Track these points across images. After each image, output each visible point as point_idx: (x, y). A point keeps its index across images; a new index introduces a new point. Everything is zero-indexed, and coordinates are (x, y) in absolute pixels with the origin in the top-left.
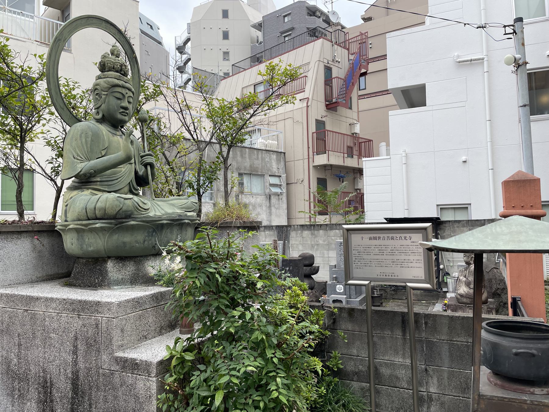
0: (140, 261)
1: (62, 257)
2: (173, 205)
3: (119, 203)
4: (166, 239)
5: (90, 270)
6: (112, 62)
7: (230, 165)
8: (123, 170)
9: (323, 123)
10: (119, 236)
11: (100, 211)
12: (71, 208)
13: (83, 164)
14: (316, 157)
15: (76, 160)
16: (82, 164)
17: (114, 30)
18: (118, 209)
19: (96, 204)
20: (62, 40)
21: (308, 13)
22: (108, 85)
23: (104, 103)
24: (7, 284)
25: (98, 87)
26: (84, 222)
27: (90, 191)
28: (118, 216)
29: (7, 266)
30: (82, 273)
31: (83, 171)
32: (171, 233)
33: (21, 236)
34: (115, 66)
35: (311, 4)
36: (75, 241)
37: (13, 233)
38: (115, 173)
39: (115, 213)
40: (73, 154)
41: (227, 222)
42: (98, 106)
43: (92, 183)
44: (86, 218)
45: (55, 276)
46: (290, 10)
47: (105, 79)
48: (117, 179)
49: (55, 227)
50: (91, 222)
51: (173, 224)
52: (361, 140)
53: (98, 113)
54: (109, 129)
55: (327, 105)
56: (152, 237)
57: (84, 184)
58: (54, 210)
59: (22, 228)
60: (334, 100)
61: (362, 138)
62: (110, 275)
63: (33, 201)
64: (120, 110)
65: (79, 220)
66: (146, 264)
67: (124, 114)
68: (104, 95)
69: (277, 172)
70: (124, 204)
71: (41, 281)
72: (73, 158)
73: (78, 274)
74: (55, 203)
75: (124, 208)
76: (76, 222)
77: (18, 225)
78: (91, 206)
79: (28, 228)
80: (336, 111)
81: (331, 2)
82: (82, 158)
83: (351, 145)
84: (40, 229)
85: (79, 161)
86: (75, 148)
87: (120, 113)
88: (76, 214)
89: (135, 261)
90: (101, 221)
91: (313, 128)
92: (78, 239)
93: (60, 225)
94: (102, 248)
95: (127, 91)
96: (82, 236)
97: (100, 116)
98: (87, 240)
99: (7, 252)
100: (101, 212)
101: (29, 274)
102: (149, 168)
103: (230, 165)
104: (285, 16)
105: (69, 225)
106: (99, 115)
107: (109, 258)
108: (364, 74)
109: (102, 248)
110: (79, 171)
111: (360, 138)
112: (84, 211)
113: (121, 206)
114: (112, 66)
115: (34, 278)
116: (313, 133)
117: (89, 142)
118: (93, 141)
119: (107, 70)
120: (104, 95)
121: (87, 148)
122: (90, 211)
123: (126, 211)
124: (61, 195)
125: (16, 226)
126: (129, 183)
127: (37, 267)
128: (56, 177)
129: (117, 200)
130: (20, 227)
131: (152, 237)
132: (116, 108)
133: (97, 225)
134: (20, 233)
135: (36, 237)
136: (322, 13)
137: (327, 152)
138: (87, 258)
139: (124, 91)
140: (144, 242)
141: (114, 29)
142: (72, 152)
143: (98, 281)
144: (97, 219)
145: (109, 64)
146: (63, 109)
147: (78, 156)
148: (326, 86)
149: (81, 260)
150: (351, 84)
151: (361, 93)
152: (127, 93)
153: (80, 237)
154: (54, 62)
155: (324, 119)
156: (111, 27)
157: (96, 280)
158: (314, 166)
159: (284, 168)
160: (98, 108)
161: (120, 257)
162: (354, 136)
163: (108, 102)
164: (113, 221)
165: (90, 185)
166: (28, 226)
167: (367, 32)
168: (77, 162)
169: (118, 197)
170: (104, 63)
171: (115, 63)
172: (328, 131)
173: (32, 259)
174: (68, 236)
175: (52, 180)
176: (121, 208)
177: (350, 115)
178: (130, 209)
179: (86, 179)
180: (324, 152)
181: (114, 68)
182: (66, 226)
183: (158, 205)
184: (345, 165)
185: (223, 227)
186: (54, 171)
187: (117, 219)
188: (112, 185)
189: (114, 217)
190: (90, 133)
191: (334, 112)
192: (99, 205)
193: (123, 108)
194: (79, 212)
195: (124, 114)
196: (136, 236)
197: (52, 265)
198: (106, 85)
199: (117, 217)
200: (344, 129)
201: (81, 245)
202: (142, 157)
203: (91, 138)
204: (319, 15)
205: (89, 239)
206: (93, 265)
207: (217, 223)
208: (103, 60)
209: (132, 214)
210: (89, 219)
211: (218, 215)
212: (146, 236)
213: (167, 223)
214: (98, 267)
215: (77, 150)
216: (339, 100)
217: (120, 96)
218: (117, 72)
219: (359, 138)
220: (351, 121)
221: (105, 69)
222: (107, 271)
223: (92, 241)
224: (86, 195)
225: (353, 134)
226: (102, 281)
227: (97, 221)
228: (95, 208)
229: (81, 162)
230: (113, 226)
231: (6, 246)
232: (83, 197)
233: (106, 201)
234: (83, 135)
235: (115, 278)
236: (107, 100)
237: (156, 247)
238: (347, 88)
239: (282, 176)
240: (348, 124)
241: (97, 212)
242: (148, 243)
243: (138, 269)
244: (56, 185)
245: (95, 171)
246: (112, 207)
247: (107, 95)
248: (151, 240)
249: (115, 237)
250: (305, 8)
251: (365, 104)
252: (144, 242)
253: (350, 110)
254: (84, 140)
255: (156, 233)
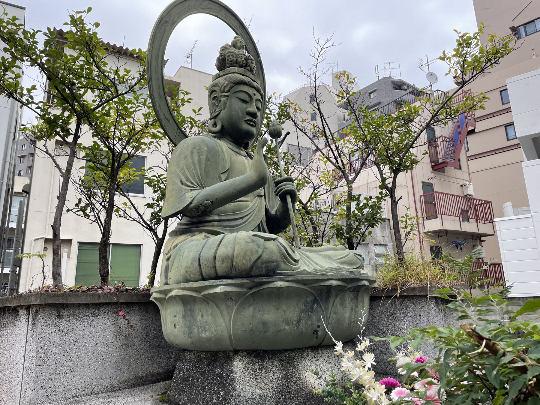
0: (291, 359)
1: (159, 346)
2: (329, 257)
3: (255, 247)
4: (335, 316)
5: (203, 374)
6: (235, 53)
7: (401, 198)
8: (251, 204)
9: (431, 185)
10: (254, 309)
11: (223, 263)
12: (175, 261)
13: (195, 193)
14: (426, 222)
15: (184, 187)
16: (193, 192)
17: (236, 23)
18: (254, 258)
19: (217, 250)
20: (170, 23)
21: (394, 87)
22: (230, 82)
23: (224, 108)
24: (71, 396)
25: (215, 88)
26: (197, 284)
27: (204, 234)
28: (255, 272)
29: (74, 362)
30: (189, 380)
31: (194, 202)
32: (343, 304)
33: (99, 312)
34: (239, 59)
35: (396, 79)
36: (179, 319)
37: (87, 305)
38: (239, 209)
39: (249, 265)
40: (180, 178)
41: (414, 289)
42: (215, 114)
43: (207, 224)
44: (198, 276)
45: (148, 379)
46: (376, 87)
47: (224, 77)
48: (242, 218)
49: (150, 296)
50: (207, 283)
51: (346, 287)
52: (476, 203)
53: (215, 125)
54: (230, 146)
55: (433, 167)
56: (312, 312)
57: (194, 226)
58: (151, 271)
59: (101, 298)
60: (440, 161)
61: (477, 199)
62: (239, 387)
63: (139, 277)
64: (245, 117)
65: (188, 281)
66: (301, 366)
67: (251, 123)
68: (224, 96)
69: (382, 240)
70: (265, 248)
71: (125, 388)
72: (180, 184)
73: (182, 382)
74: (153, 262)
75: (265, 256)
76: (183, 285)
77: (97, 292)
78: (208, 254)
79: (111, 299)
80: (444, 172)
81: (427, 64)
82: (193, 184)
83: (465, 208)
84: (129, 300)
85: (189, 188)
86: (183, 169)
87: (246, 121)
88: (183, 271)
89: (281, 360)
90: (225, 281)
91: (420, 191)
92: (184, 317)
93: (156, 292)
94: (226, 334)
95: (255, 92)
96: (191, 310)
97: (219, 127)
98: (199, 318)
99: (74, 339)
100: (224, 265)
101: (107, 376)
102: (289, 199)
103: (401, 198)
104: (370, 93)
105: (170, 291)
106: (216, 126)
107: (236, 352)
108: (472, 132)
109: (226, 334)
110: (189, 202)
111: (475, 199)
112: (197, 263)
113: (260, 251)
114: (235, 59)
115: (115, 383)
116: (420, 196)
117: (204, 161)
118: (209, 160)
119: (227, 65)
120: (224, 96)
121: (201, 169)
122: (205, 263)
123: (268, 262)
124: (162, 251)
125: (93, 295)
126: (259, 224)
127: (120, 364)
128: (156, 226)
129: (253, 241)
130: (99, 296)
131: (312, 312)
132: (241, 115)
133: (218, 290)
134: (98, 306)
135: (121, 313)
136: (408, 86)
137: (439, 216)
138: (198, 351)
139: (251, 91)
140: (299, 322)
141: (236, 20)
142: (178, 175)
143: (218, 399)
144: (217, 277)
145: (231, 57)
146: (168, 121)
147: (187, 180)
148: (430, 147)
149: (188, 355)
150: (459, 143)
151: (469, 154)
152: (254, 94)
153: (189, 313)
154: (159, 51)
155: (431, 181)
156: (232, 18)
157: (214, 397)
158: (425, 233)
159: (390, 236)
160: (215, 117)
161: (255, 351)
162: (468, 197)
163: (230, 105)
164: (245, 281)
165: (204, 226)
166: (112, 294)
167: (470, 90)
168: (185, 190)
169: (254, 235)
170: (225, 56)
171: (238, 55)
172: (436, 192)
173: (115, 350)
174: (169, 311)
175: (151, 229)
176: (261, 256)
177: (461, 175)
178: (275, 258)
179: (199, 216)
180: (435, 216)
181: (237, 63)
182: (166, 292)
183: (308, 257)
184: (463, 230)
185: (407, 297)
186: (155, 218)
187: (252, 276)
188: (236, 226)
189: (247, 274)
190: (206, 148)
191: (442, 173)
192: (222, 251)
193: (249, 114)
194: (187, 267)
195: (251, 123)
196: (284, 311)
197: (144, 361)
198: (227, 83)
199: (253, 274)
200: (456, 190)
201: (190, 328)
202: (277, 183)
203: (207, 156)
204: (406, 88)
205: (202, 316)
206: (208, 366)
207: (395, 289)
208: (223, 52)
209: (278, 267)
210: (203, 279)
211: (393, 276)
212: (302, 311)
213: (338, 286)
214: (217, 370)
215: (187, 173)
216: (447, 160)
217: (247, 98)
218: (241, 66)
219: (474, 199)
220: (463, 182)
221: (224, 66)
222: (233, 380)
223: (208, 319)
224: (198, 240)
225: (466, 196)
226: (224, 399)
227: (218, 282)
228: (215, 257)
229: (192, 190)
230: (245, 290)
231: (75, 328)
232: (194, 243)
233: (235, 244)
234: (195, 151)
235: (249, 396)
236: (228, 104)
237: (320, 333)
238: (454, 147)
239: (388, 244)
240: (459, 185)
241: (218, 264)
242: (306, 323)
243: (288, 377)
244: (157, 236)
245: (212, 202)
246: (245, 254)
247: (228, 96)
248: (310, 318)
249: (249, 311)
250: (391, 83)
251: (475, 165)
252: (299, 322)
253: (459, 171)
254: (196, 158)
255: (319, 304)
